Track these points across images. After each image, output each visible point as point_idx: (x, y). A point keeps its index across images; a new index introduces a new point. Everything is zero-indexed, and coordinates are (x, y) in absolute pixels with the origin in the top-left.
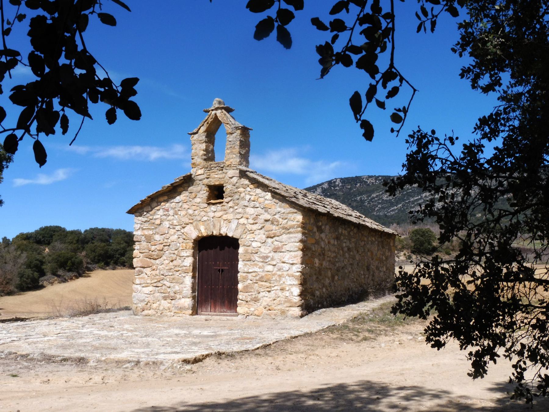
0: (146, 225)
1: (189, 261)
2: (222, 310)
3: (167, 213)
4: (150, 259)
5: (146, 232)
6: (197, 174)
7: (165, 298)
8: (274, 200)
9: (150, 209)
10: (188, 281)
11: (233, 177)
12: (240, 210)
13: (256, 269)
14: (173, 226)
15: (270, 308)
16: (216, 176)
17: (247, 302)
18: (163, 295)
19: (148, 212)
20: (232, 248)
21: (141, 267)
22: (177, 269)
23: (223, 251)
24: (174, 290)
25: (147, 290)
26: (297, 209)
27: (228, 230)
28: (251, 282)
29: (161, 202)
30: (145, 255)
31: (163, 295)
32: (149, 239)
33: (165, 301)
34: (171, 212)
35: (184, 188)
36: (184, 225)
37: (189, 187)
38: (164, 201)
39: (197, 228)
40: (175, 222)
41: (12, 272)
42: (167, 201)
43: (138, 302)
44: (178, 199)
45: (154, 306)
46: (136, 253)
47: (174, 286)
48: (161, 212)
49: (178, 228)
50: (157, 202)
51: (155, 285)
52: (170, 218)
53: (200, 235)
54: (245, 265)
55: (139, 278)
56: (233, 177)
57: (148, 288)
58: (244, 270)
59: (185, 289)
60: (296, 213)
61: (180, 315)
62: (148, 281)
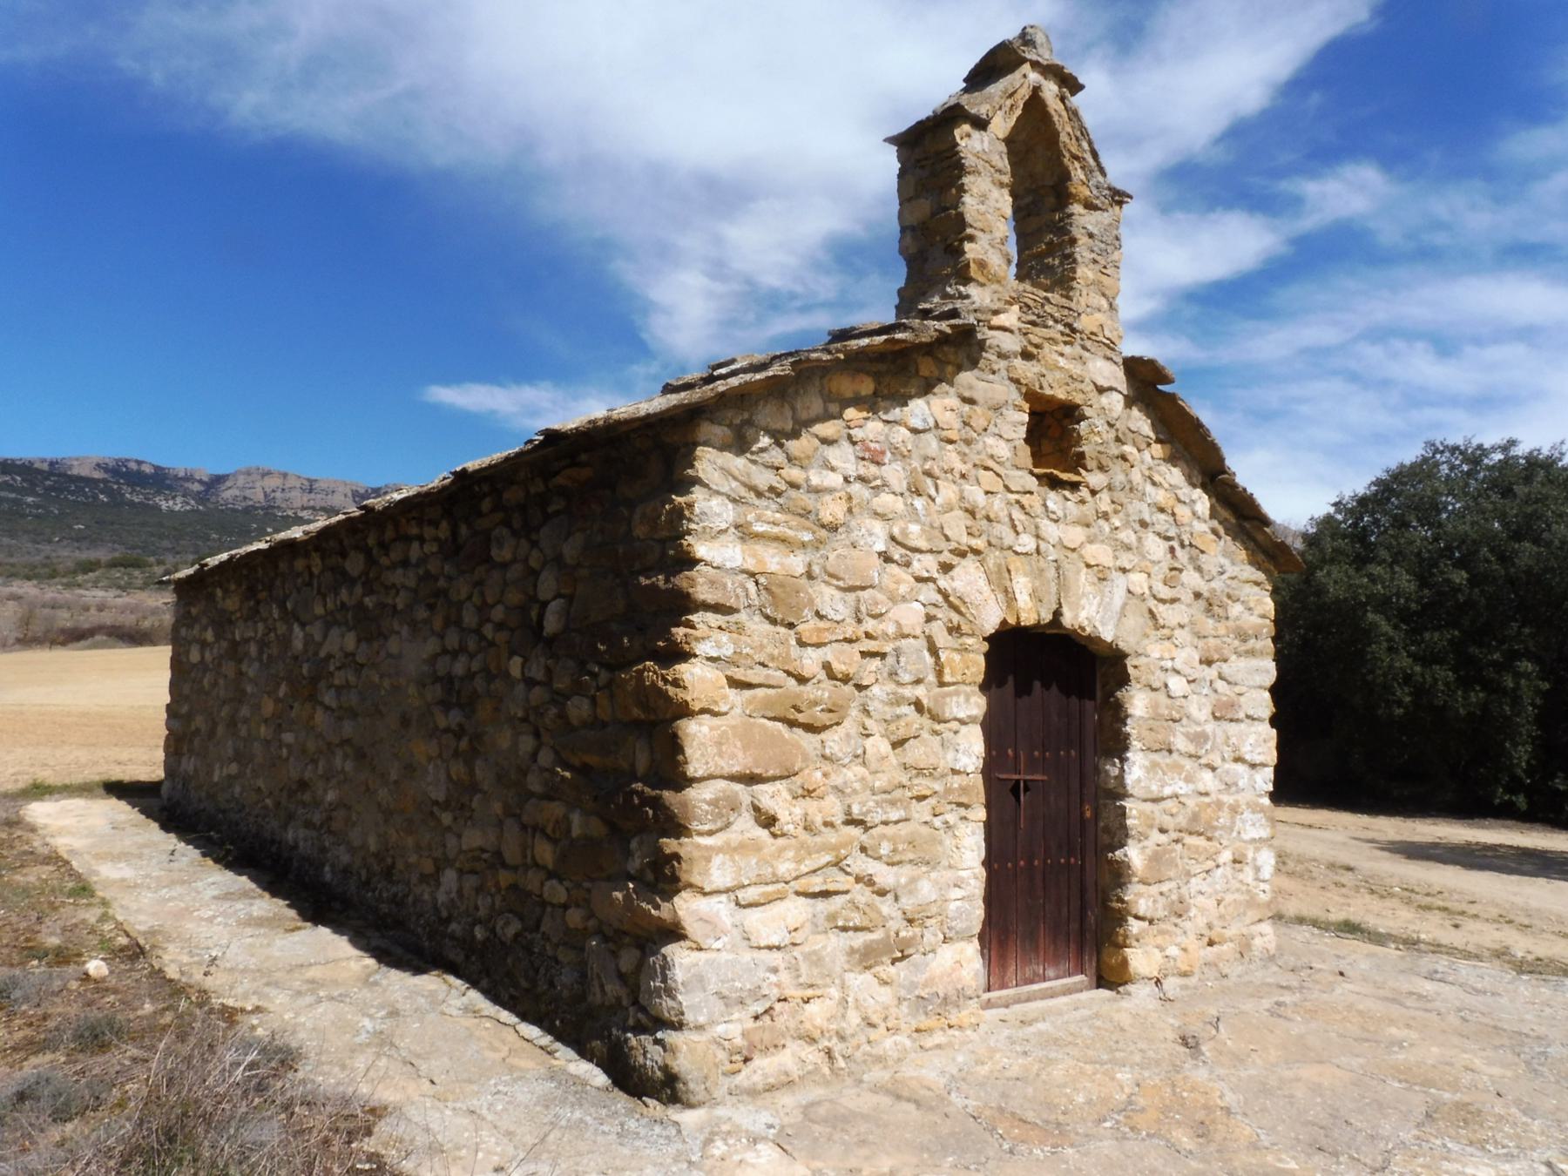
0: (765, 517)
1: (971, 749)
2: (1028, 973)
3: (873, 469)
4: (792, 724)
5: (773, 560)
6: (996, 321)
7: (866, 958)
8: (1215, 523)
9: (789, 426)
10: (968, 846)
11: (1111, 389)
12: (1127, 536)
13: (1181, 787)
14: (898, 552)
15: (1213, 935)
16: (1062, 362)
17: (1151, 922)
18: (859, 940)
19: (779, 438)
20: (1054, 689)
21: (733, 778)
22: (923, 785)
23: (1026, 699)
24: (907, 902)
25: (769, 924)
26: (1265, 571)
27: (1093, 613)
28: (1163, 838)
29: (846, 403)
30: (768, 704)
31: (859, 940)
32: (781, 606)
33: (868, 976)
34: (894, 473)
35: (942, 363)
36: (947, 557)
37: (960, 368)
38: (857, 402)
39: (1001, 583)
40: (915, 534)
41: (96, 1036)
42: (871, 404)
43: (719, 1006)
44: (918, 410)
45: (817, 1013)
46: (697, 678)
47: (913, 880)
48: (843, 458)
49: (925, 564)
50: (828, 398)
51: (817, 884)
52: (885, 501)
53: (1012, 621)
54: (1154, 765)
55: (727, 849)
56: (1111, 389)
57: (777, 908)
58: (1147, 788)
59: (958, 893)
60: (1257, 584)
61: (939, 1038)
62: (785, 868)
